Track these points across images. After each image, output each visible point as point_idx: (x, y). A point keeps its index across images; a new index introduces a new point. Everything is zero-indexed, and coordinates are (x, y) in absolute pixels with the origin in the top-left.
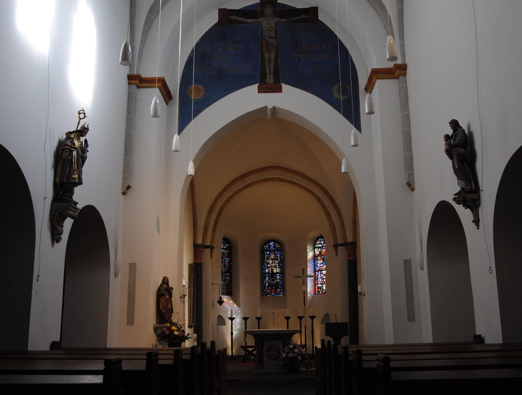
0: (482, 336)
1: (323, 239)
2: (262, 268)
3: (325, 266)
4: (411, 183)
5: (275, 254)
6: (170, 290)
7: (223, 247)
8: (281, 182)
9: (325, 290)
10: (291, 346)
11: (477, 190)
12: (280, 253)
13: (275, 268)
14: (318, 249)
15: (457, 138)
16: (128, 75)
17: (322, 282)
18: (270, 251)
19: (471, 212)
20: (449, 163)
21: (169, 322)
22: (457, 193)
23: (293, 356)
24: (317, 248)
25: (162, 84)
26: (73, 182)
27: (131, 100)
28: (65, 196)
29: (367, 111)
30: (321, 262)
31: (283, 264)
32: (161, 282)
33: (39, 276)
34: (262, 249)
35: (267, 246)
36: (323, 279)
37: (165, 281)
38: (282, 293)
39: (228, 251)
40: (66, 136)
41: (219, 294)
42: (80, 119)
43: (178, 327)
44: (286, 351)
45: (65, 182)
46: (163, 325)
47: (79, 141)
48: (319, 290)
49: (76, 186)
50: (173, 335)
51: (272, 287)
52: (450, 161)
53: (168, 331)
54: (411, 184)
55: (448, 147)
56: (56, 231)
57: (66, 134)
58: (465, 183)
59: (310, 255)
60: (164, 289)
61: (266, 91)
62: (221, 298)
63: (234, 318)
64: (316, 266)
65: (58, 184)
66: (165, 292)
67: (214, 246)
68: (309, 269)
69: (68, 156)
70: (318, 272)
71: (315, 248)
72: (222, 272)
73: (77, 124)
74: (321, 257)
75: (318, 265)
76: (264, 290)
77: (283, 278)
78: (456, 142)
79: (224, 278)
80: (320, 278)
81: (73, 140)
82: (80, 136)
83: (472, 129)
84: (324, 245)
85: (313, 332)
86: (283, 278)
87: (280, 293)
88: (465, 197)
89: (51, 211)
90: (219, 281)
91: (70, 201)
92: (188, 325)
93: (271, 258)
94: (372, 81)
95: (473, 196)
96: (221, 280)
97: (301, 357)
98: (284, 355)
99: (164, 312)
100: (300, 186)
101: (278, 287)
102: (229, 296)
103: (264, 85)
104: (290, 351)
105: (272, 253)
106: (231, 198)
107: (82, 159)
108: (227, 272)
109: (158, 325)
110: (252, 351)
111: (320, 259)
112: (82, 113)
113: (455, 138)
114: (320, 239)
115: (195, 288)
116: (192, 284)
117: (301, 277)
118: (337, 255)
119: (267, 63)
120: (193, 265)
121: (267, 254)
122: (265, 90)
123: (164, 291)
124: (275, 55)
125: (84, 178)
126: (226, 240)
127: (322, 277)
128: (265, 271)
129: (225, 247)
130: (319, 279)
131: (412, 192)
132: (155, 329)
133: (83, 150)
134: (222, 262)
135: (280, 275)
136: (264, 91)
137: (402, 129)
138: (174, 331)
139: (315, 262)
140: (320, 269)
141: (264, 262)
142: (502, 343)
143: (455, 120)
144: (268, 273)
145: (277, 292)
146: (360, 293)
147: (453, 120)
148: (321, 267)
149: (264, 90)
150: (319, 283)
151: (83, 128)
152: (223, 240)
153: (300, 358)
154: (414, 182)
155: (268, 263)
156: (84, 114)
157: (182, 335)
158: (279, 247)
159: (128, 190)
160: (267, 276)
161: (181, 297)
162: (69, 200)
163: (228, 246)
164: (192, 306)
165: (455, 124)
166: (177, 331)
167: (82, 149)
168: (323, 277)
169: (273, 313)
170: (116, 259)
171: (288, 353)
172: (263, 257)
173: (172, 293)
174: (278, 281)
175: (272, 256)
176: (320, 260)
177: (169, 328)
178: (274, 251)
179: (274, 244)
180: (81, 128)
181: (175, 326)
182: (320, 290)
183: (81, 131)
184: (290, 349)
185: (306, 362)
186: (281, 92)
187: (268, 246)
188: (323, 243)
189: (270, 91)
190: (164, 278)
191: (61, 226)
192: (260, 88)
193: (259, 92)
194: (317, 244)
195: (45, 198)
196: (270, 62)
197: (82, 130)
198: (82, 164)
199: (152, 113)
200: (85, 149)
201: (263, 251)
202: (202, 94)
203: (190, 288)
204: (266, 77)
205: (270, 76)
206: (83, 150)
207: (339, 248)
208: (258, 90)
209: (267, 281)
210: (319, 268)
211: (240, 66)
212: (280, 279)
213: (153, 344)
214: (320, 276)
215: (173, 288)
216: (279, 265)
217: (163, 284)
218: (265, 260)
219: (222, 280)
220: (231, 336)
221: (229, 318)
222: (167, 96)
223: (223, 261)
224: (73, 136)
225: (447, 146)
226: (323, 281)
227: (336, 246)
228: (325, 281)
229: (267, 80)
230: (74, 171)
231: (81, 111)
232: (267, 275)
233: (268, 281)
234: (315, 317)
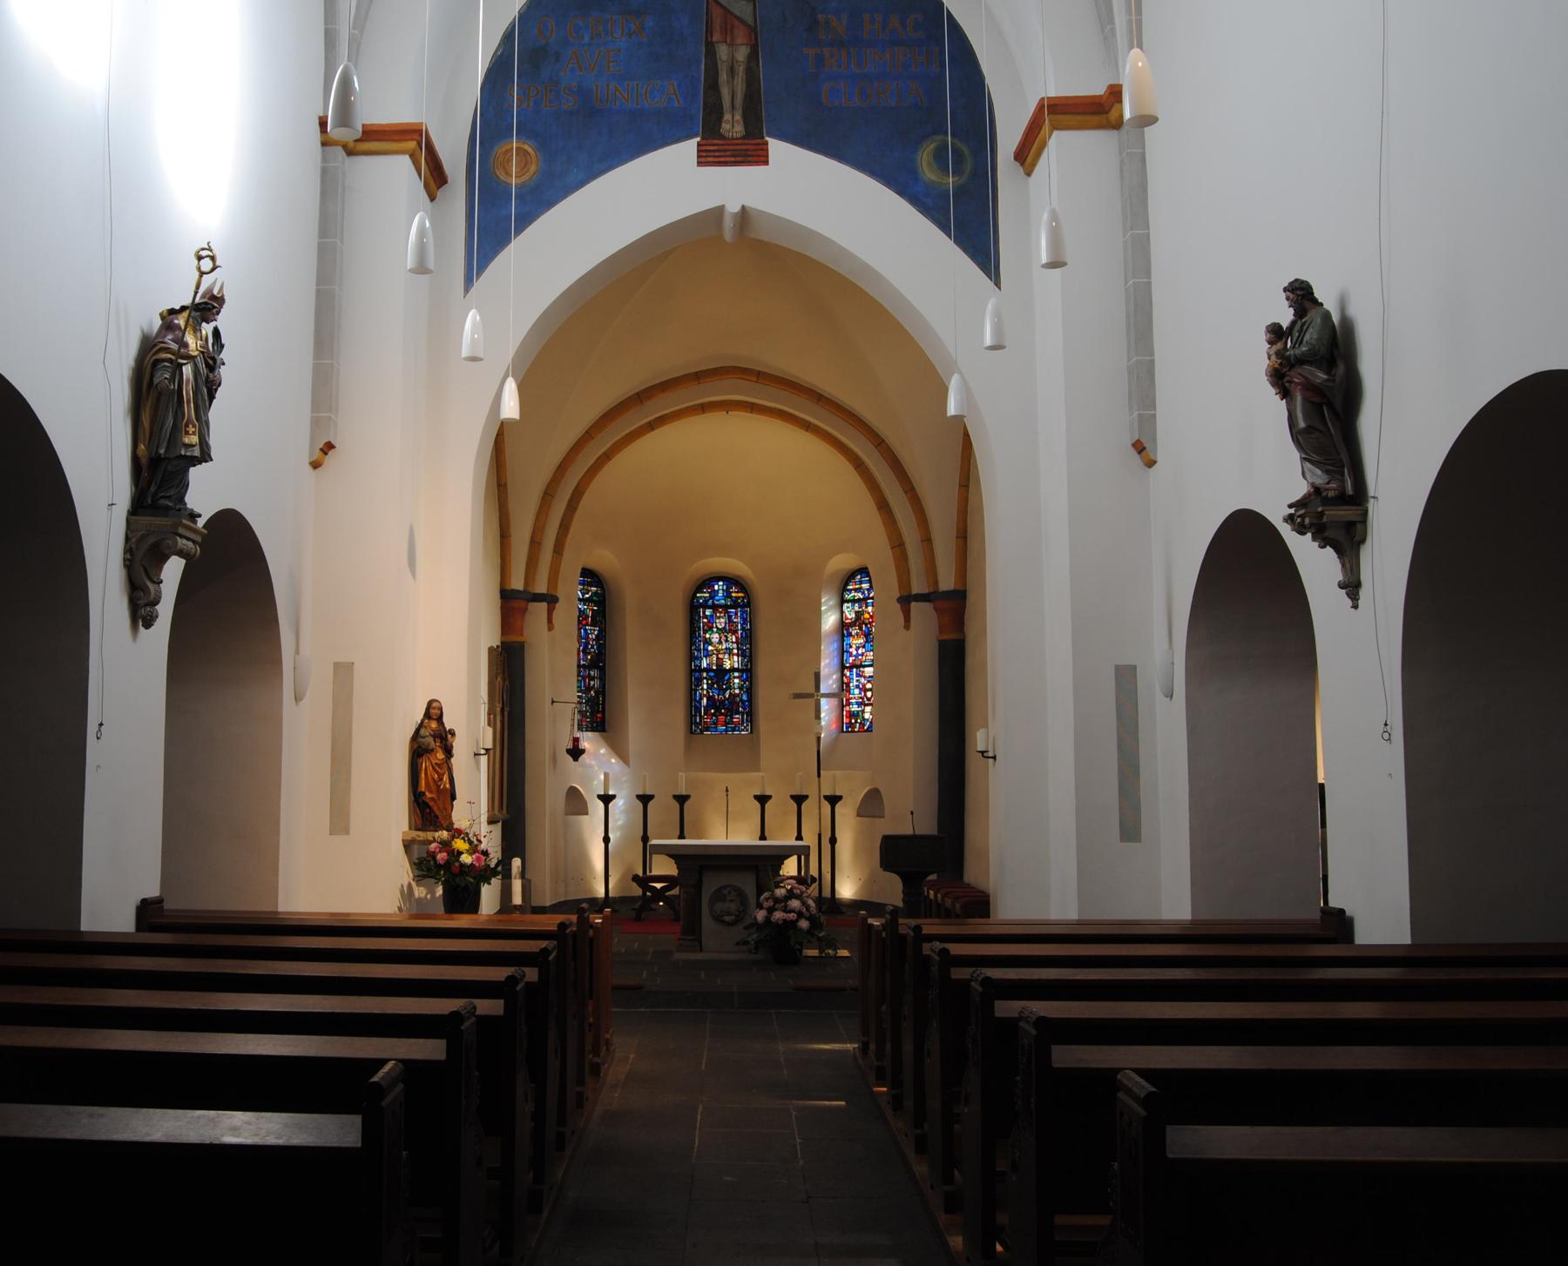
0: (1348, 913)
3: (872, 653)
4: (1146, 445)
5: (730, 617)
6: (446, 736)
7: (581, 597)
8: (751, 412)
9: (871, 723)
10: (780, 892)
11: (1358, 497)
12: (743, 612)
13: (727, 656)
15: (1305, 339)
17: (861, 698)
18: (715, 607)
19: (1336, 556)
20: (1274, 410)
21: (444, 826)
22: (1298, 501)
23: (785, 921)
24: (848, 601)
26: (185, 457)
27: (330, 190)
28: (164, 497)
29: (1044, 259)
30: (861, 641)
31: (751, 645)
32: (422, 717)
33: (101, 725)
34: (692, 602)
36: (866, 690)
37: (433, 712)
39: (595, 608)
40: (160, 322)
41: (572, 731)
42: (202, 274)
43: (470, 842)
44: (766, 905)
45: (162, 456)
46: (428, 833)
47: (199, 334)
48: (853, 721)
49: (194, 465)
50: (457, 864)
51: (718, 709)
52: (1281, 406)
53: (445, 854)
54: (1144, 448)
55: (1279, 361)
56: (142, 594)
57: (161, 315)
58: (1322, 471)
59: (830, 621)
61: (722, 159)
62: (576, 740)
63: (613, 797)
64: (845, 654)
65: (144, 461)
66: (433, 743)
67: (558, 595)
68: (826, 659)
69: (170, 381)
71: (843, 601)
72: (579, 666)
73: (194, 288)
74: (861, 629)
76: (696, 716)
78: (1304, 349)
79: (585, 682)
80: (857, 687)
81: (184, 334)
82: (200, 320)
83: (1354, 311)
85: (833, 841)
86: (751, 683)
88: (1322, 514)
89: (127, 539)
90: (571, 693)
91: (179, 510)
92: (488, 818)
93: (717, 627)
94: (1039, 133)
95: (1345, 513)
96: (575, 689)
97: (808, 922)
98: (761, 915)
99: (432, 799)
100: (807, 426)
101: (734, 708)
102: (596, 734)
103: (715, 142)
104: (777, 906)
105: (720, 612)
106: (607, 457)
107: (209, 387)
109: (414, 834)
111: (857, 634)
112: (207, 256)
113: (1299, 336)
114: (859, 577)
115: (506, 713)
116: (497, 705)
117: (809, 696)
118: (907, 626)
119: (723, 76)
120: (500, 649)
121: (705, 617)
122: (717, 157)
123: (431, 740)
124: (749, 50)
125: (213, 441)
126: (590, 576)
127: (861, 686)
129: (587, 596)
130: (852, 692)
131: (1148, 469)
132: (408, 846)
133: (211, 362)
134: (579, 636)
136: (717, 160)
137: (1126, 283)
138: (462, 853)
139: (843, 641)
140: (858, 663)
141: (697, 638)
142: (1409, 942)
143: (1303, 282)
144: (708, 670)
145: (733, 723)
147: (1296, 280)
148: (860, 657)
149: (714, 157)
150: (853, 701)
151: (208, 296)
153: (804, 924)
154: (1155, 440)
155: (708, 642)
156: (213, 258)
157: (483, 864)
158: (739, 598)
159: (326, 454)
160: (705, 678)
162: (177, 507)
163: (595, 594)
164: (497, 766)
165: (1303, 296)
166: (471, 854)
167: (209, 360)
168: (864, 685)
169: (727, 791)
170: (297, 652)
171: (771, 910)
173: (452, 746)
174: (737, 691)
175: (721, 622)
177: (446, 845)
178: (726, 607)
179: (725, 587)
180: (203, 296)
181: (463, 838)
182: (856, 722)
183: (204, 306)
184: (777, 900)
185: (821, 935)
186: (766, 163)
187: (708, 592)
188: (867, 589)
189: (733, 159)
190: (430, 703)
191: (156, 580)
192: (702, 151)
193: (700, 164)
194: (850, 591)
195: (109, 505)
196: (732, 71)
197: (205, 303)
198: (207, 403)
199: (410, 262)
200: (216, 356)
201: (693, 608)
202: (533, 168)
203: (492, 716)
204: (720, 118)
205: (733, 115)
206: (211, 361)
207: (915, 607)
208: (699, 157)
209: (705, 692)
211: (645, 87)
212: (741, 688)
213: (402, 886)
214: (855, 683)
216: (738, 649)
217: (426, 721)
218: (699, 634)
219: (578, 687)
221: (600, 797)
222: (435, 177)
224: (181, 321)
225: (1273, 358)
226: (865, 695)
227: (906, 600)
229: (725, 127)
230: (187, 426)
231: (203, 249)
232: (705, 675)
233: (708, 692)
234: (840, 798)
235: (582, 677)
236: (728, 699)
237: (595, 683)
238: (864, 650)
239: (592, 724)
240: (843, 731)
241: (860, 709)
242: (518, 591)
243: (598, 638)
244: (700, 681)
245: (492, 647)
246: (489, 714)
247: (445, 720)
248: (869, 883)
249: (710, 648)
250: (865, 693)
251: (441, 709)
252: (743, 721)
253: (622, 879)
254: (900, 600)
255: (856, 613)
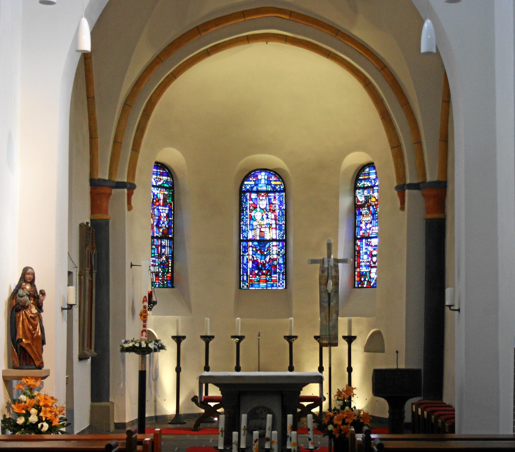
1: (374, 168)
3: (377, 228)
5: (270, 200)
9: (376, 280)
13: (267, 229)
17: (368, 262)
18: (258, 192)
24: (360, 188)
35: (251, 181)
38: (283, 282)
51: (260, 270)
60: (27, 295)
64: (357, 228)
71: (356, 188)
72: (153, 237)
76: (243, 275)
77: (286, 250)
80: (366, 253)
93: (260, 208)
99: (28, 344)
105: (263, 196)
106: (174, 76)
108: (165, 236)
110: (217, 407)
116: (87, 268)
118: (402, 208)
120: (89, 225)
121: (251, 199)
124: (252, 193)
130: (361, 257)
139: (355, 218)
146: (450, 306)
148: (368, 231)
152: (154, 168)
158: (277, 185)
160: (251, 246)
161: (63, 309)
163: (167, 182)
164: (87, 309)
168: (371, 252)
172: (242, 205)
173: (42, 304)
174: (275, 256)
176: (366, 214)
178: (267, 192)
182: (365, 280)
188: (374, 179)
194: (361, 180)
201: (242, 193)
203: (82, 277)
209: (251, 257)
210: (363, 232)
214: (364, 251)
216: (276, 224)
223: (154, 214)
226: (372, 260)
227: (401, 189)
228: (376, 262)
233: (253, 257)
235: (156, 246)
236: (268, 263)
237: (166, 251)
238: (371, 226)
239: (163, 282)
240: (355, 287)
241: (368, 270)
242: (104, 180)
243: (168, 216)
244: (246, 248)
245: (83, 223)
246: (80, 276)
247: (36, 283)
248: (371, 404)
249: (255, 223)
250: (372, 258)
251: (33, 274)
252: (279, 279)
253: (186, 400)
254: (397, 188)
255: (366, 197)
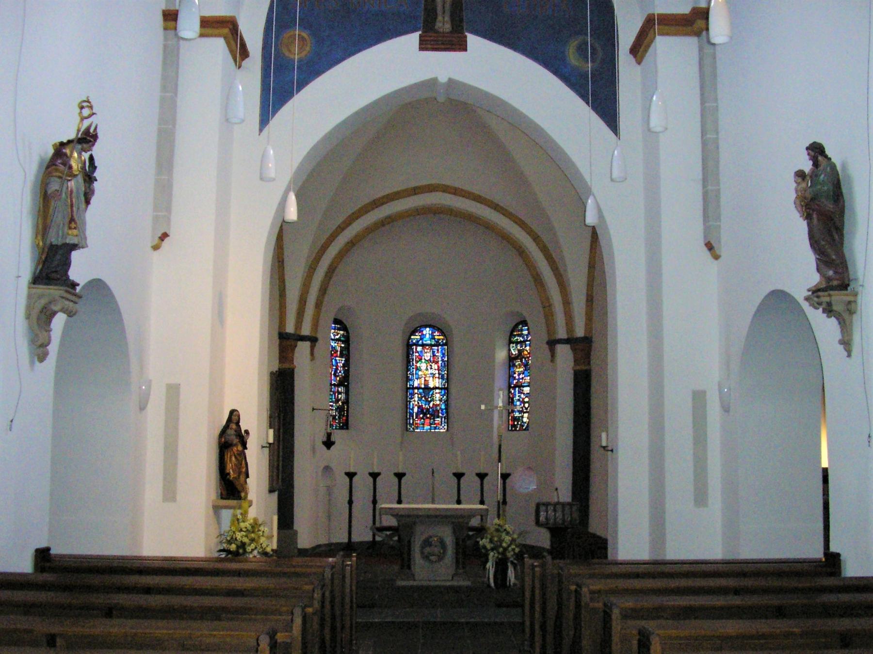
1: (526, 325)
2: (408, 377)
3: (529, 378)
5: (433, 352)
9: (528, 424)
14: (516, 345)
16: (164, 12)
18: (423, 345)
25: (230, 29)
36: (524, 403)
48: (516, 423)
51: (425, 414)
62: (329, 435)
70: (515, 390)
75: (515, 375)
76: (410, 419)
79: (335, 396)
80: (519, 400)
84: (529, 339)
87: (441, 425)
93: (425, 359)
121: (417, 352)
127: (521, 400)
128: (413, 383)
130: (515, 403)
135: (441, 392)
139: (510, 370)
141: (411, 366)
147: (815, 143)
148: (521, 380)
155: (417, 369)
156: (91, 107)
161: (263, 447)
163: (343, 335)
168: (523, 399)
174: (438, 402)
175: (428, 356)
178: (431, 345)
194: (515, 336)
202: (308, 49)
214: (517, 398)
215: (249, 431)
216: (439, 374)
220: (348, 505)
222: (240, 52)
227: (552, 344)
229: (438, 25)
233: (418, 403)
